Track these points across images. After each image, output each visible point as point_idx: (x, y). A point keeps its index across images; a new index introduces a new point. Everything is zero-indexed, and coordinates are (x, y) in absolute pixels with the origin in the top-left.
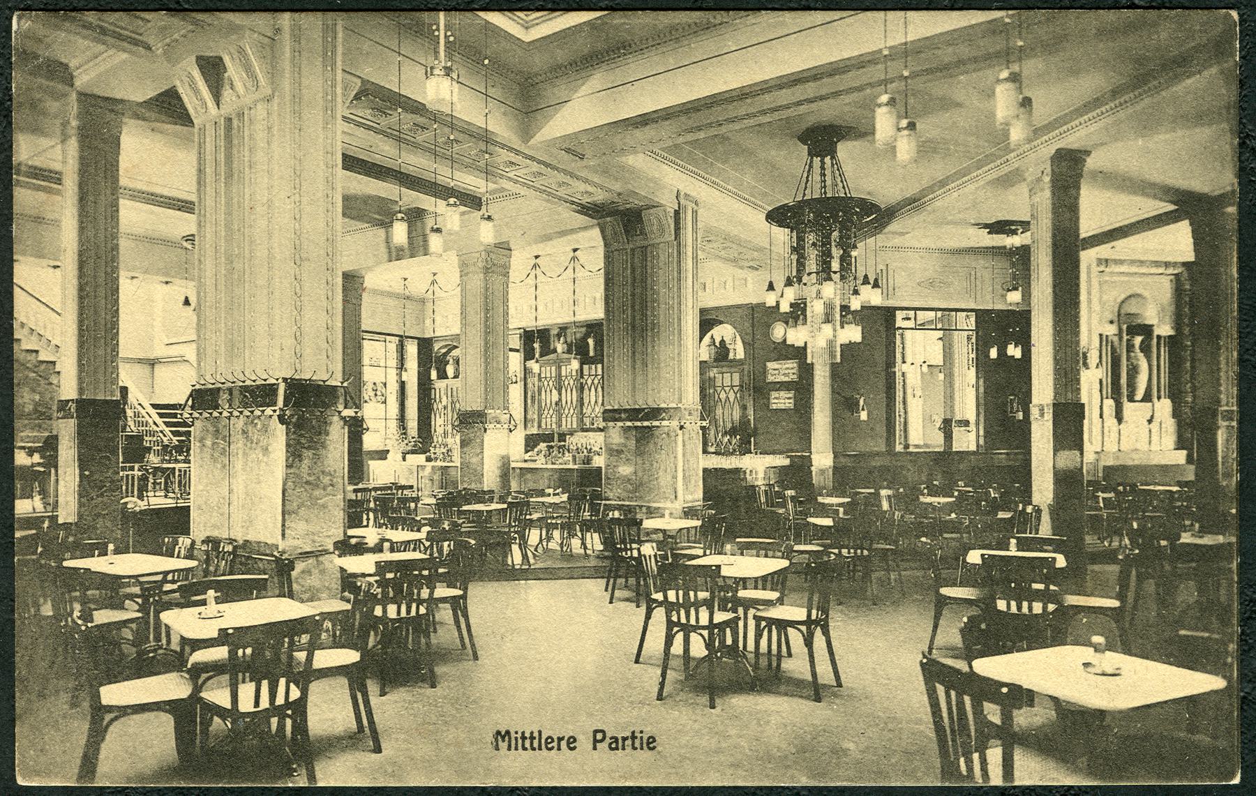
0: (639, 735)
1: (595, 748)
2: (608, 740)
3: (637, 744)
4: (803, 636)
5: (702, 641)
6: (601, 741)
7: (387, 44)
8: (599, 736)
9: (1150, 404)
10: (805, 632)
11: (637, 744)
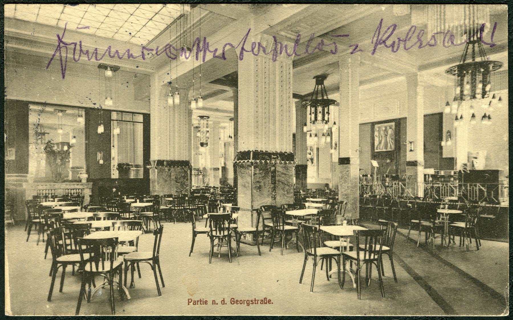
0: (202, 300)
1: (224, 299)
2: (193, 302)
3: (202, 303)
4: (151, 265)
5: (150, 266)
6: (190, 302)
7: (506, 241)
8: (190, 301)
9: (340, 157)
10: (152, 264)
11: (202, 303)
